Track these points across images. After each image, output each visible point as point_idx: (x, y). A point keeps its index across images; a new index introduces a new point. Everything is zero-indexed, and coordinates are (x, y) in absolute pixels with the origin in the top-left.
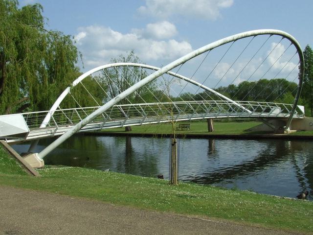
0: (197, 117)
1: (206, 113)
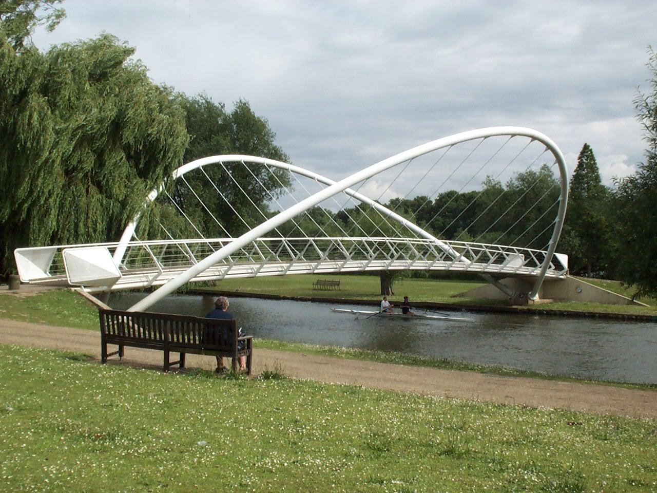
0: (352, 265)
1: (452, 260)
